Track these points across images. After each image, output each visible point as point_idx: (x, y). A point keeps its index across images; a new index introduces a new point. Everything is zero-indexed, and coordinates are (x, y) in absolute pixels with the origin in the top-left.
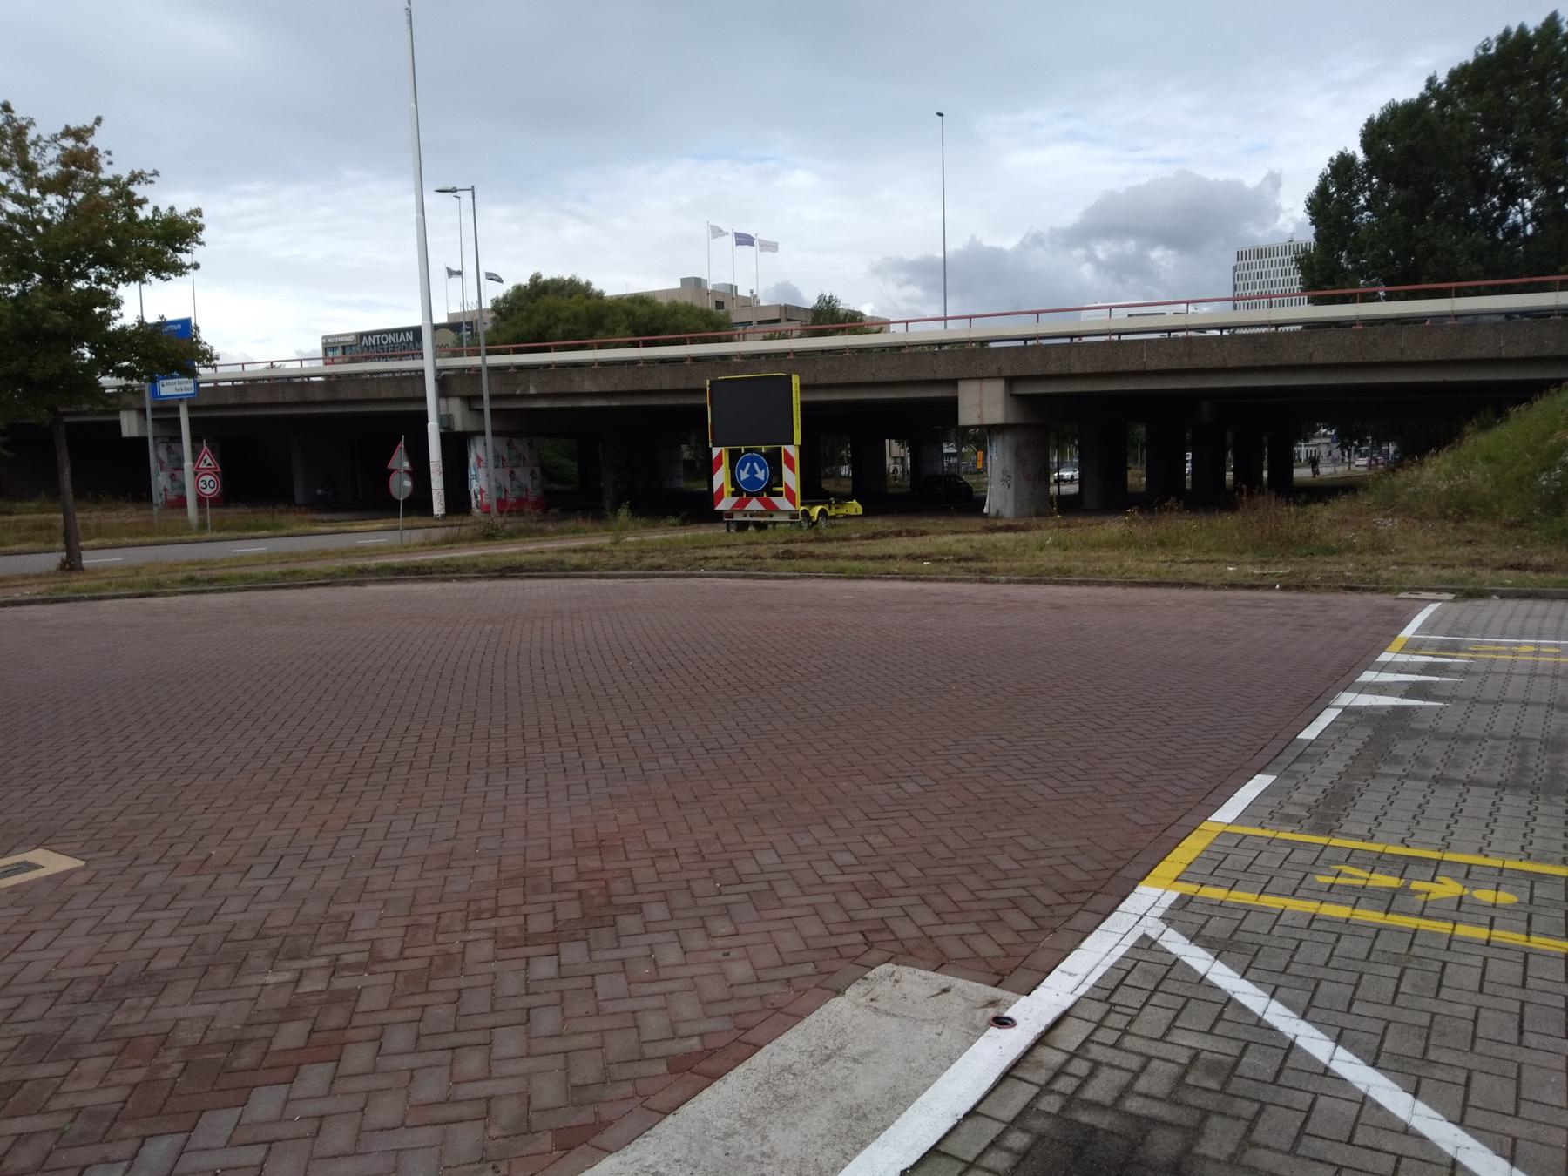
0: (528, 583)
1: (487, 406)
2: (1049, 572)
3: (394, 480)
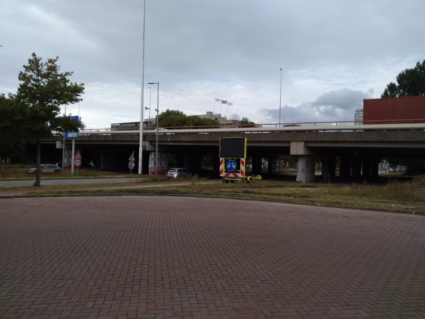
1: (157, 144)
2: (333, 203)
3: (130, 163)
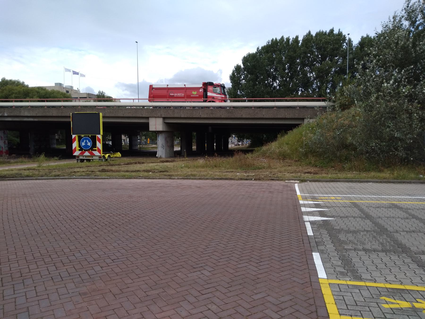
0: (9, 182)
2: (189, 176)
